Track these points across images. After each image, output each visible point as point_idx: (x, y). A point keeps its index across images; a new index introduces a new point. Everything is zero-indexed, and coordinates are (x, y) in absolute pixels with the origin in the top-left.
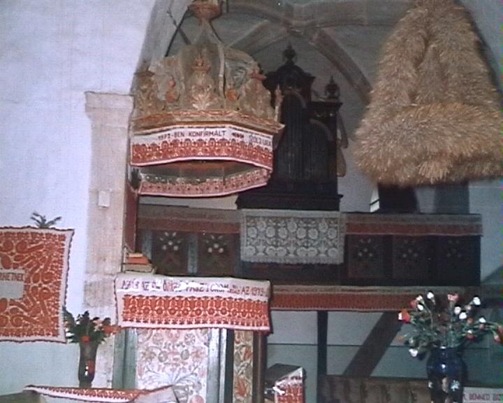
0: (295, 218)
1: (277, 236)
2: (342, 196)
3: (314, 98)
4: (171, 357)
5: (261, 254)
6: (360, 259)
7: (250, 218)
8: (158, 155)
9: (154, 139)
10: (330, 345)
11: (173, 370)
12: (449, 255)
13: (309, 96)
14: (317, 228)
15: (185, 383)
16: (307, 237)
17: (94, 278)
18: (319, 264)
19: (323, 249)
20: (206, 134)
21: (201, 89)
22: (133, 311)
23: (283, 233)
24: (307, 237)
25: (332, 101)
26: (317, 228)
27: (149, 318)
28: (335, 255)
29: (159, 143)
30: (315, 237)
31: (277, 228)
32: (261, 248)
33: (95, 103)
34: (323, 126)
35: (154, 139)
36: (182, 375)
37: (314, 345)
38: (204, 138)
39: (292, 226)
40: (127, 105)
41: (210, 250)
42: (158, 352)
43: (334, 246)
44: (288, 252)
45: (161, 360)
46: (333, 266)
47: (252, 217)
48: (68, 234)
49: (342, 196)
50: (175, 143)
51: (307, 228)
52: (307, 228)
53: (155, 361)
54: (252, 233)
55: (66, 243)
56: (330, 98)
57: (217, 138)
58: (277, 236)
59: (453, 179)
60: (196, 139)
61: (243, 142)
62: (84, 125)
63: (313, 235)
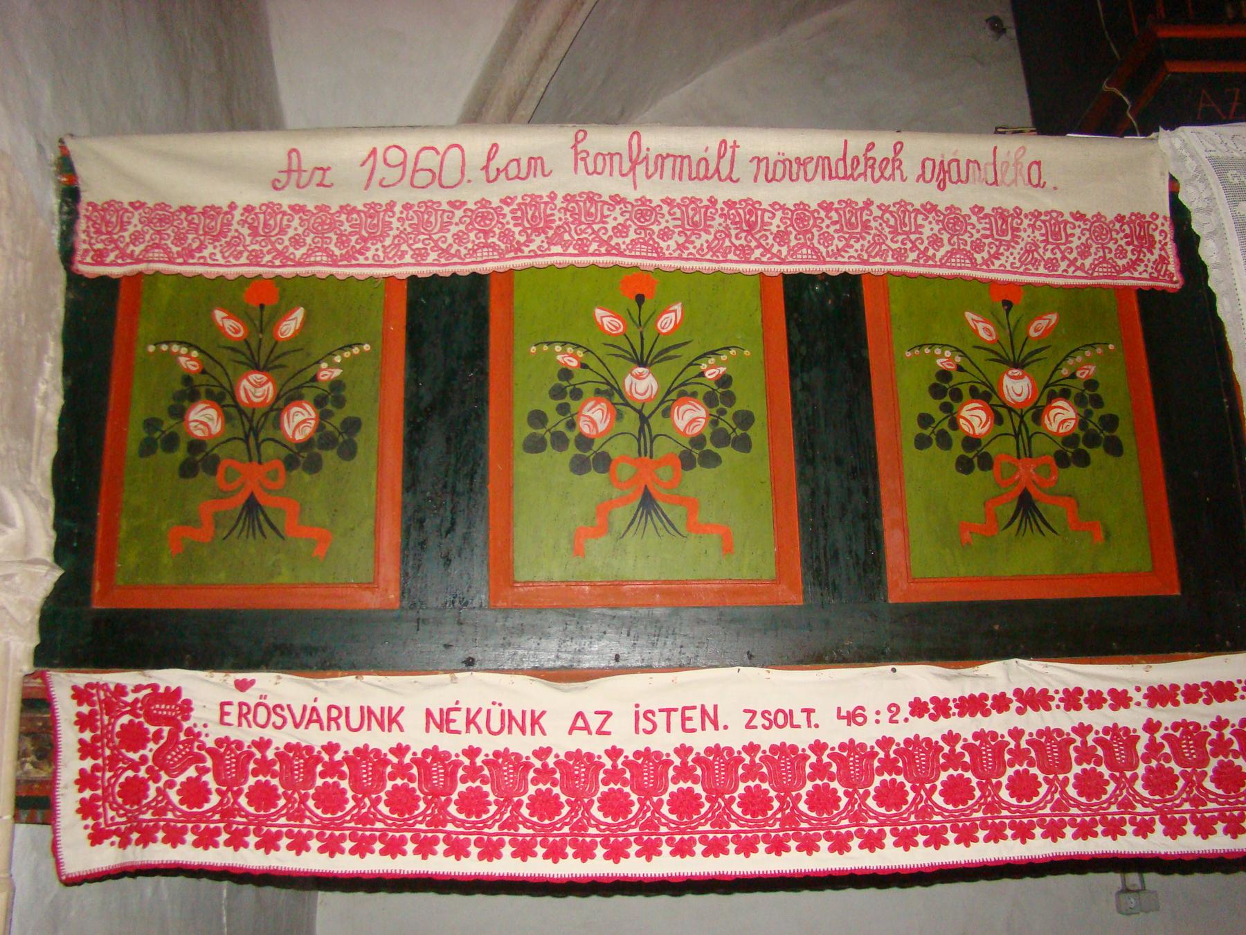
12: (204, 419)
41: (204, 419)
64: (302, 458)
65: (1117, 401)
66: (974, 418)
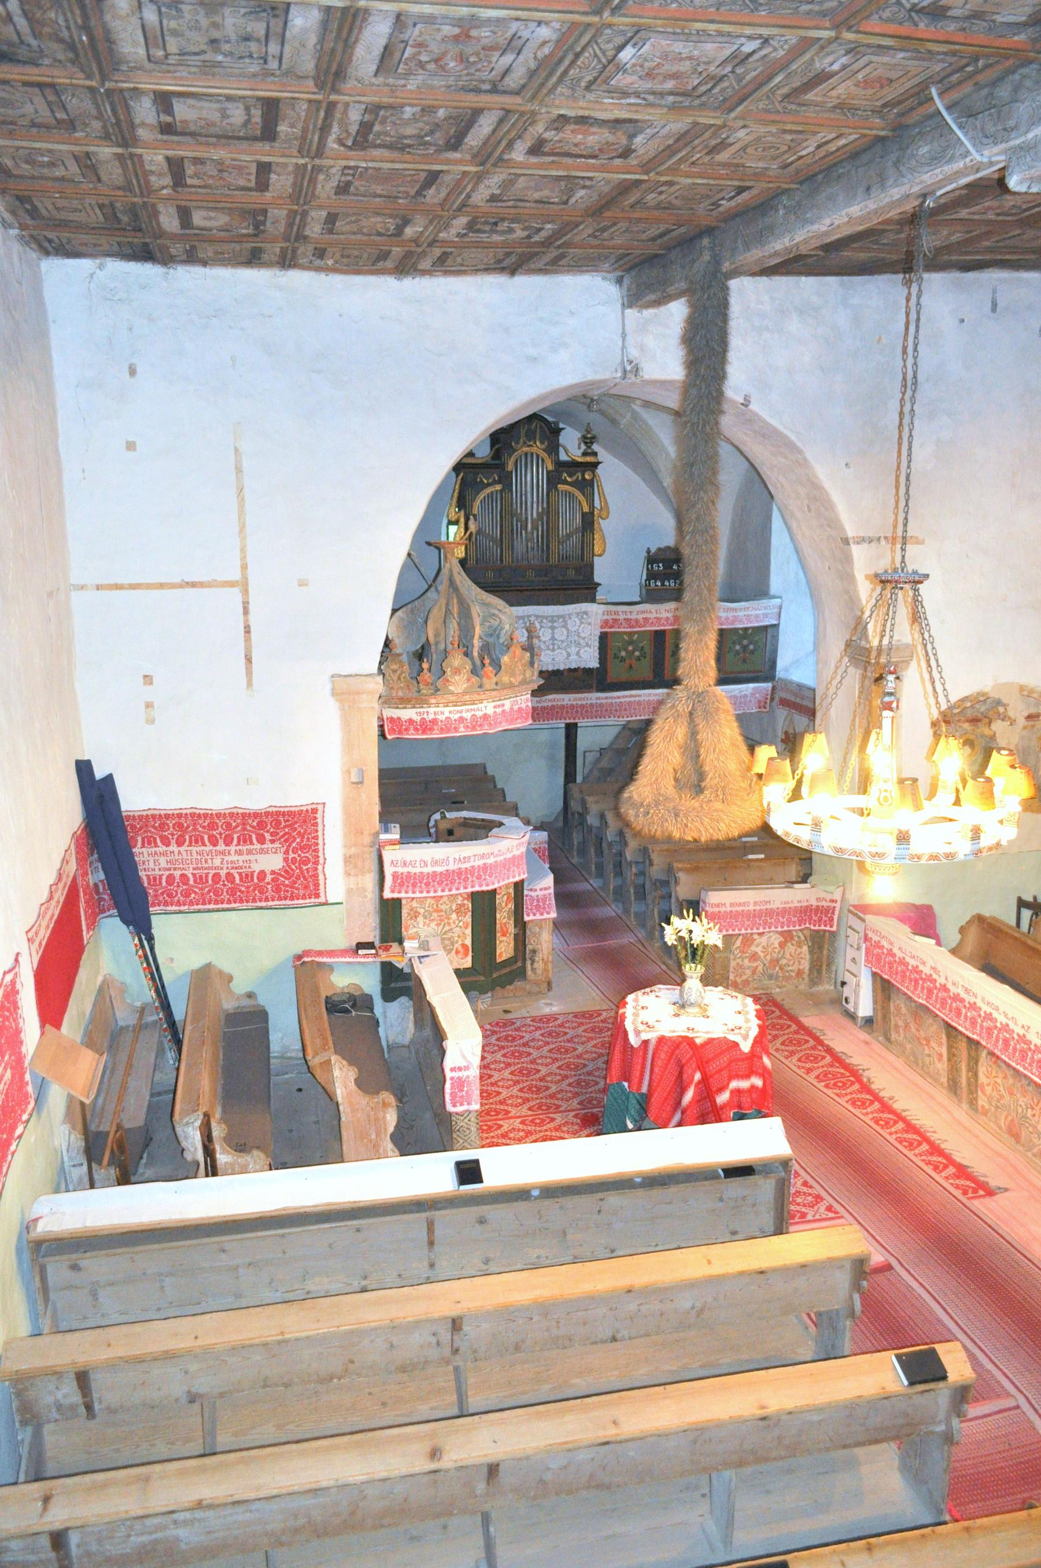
3: (563, 457)
4: (435, 915)
6: (623, 660)
8: (416, 729)
9: (407, 714)
11: (438, 925)
13: (557, 454)
14: (565, 626)
15: (450, 935)
16: (553, 638)
17: (353, 850)
18: (570, 670)
19: (573, 650)
20: (468, 711)
21: (457, 671)
22: (401, 885)
24: (553, 638)
25: (589, 459)
26: (565, 626)
27: (417, 890)
28: (590, 658)
29: (417, 718)
30: (563, 638)
33: (344, 689)
34: (577, 493)
35: (407, 714)
36: (447, 928)
38: (464, 715)
40: (377, 685)
42: (422, 911)
43: (587, 645)
44: (569, 655)
45: (425, 917)
46: (588, 671)
48: (320, 807)
50: (434, 721)
51: (553, 628)
52: (553, 628)
53: (420, 919)
55: (319, 815)
56: (585, 454)
57: (479, 714)
60: (457, 716)
61: (504, 711)
62: (331, 712)
63: (561, 634)
64: (638, 659)
65: (647, 650)
66: (623, 654)
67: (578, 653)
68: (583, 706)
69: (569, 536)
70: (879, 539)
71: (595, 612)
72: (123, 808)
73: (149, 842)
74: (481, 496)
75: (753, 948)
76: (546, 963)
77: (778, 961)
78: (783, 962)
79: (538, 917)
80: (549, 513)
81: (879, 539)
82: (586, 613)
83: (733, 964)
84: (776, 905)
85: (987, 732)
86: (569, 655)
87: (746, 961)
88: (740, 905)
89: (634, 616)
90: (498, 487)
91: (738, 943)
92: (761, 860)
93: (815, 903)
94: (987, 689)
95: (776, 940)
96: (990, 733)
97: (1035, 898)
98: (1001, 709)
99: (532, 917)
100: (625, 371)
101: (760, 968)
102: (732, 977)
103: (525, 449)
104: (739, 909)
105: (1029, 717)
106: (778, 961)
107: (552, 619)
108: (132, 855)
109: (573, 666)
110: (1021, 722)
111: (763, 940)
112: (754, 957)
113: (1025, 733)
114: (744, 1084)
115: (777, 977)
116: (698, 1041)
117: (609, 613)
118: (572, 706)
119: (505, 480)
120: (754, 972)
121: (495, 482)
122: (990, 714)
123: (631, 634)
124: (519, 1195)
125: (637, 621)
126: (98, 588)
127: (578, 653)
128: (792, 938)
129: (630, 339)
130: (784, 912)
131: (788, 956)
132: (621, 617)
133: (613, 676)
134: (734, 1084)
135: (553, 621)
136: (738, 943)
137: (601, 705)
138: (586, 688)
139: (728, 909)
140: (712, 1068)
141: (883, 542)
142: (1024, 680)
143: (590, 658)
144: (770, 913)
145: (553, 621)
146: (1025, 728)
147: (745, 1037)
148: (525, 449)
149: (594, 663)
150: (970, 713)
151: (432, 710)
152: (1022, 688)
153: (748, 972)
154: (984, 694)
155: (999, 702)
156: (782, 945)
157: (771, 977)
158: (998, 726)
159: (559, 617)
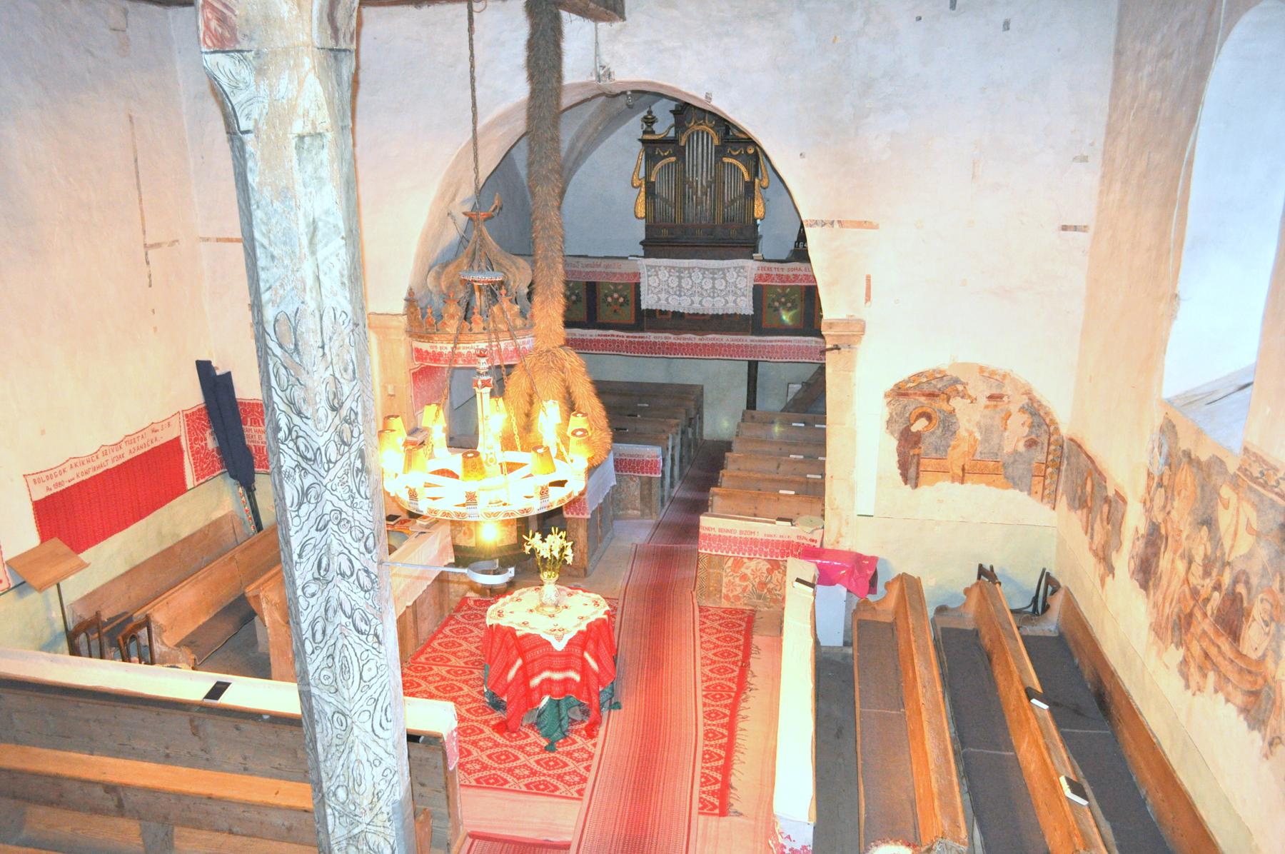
0: (700, 269)
1: (680, 286)
2: (465, 214)
5: (663, 302)
7: (649, 267)
10: (238, 240)
14: (724, 278)
16: (714, 287)
23: (686, 283)
24: (714, 287)
26: (724, 278)
28: (745, 306)
29: (430, 350)
31: (680, 278)
32: (697, 299)
37: (238, 240)
39: (697, 277)
47: (652, 267)
49: (465, 214)
51: (714, 279)
52: (714, 279)
54: (653, 281)
58: (680, 286)
59: (313, 700)
63: (720, 284)
67: (735, 302)
68: (738, 346)
69: (733, 201)
70: (832, 223)
71: (751, 267)
72: (238, 395)
73: (255, 422)
74: (659, 165)
75: (743, 570)
76: (582, 554)
77: (765, 584)
78: (771, 586)
79: (575, 516)
80: (716, 183)
81: (832, 223)
82: (743, 268)
83: (725, 580)
84: (760, 536)
85: (945, 406)
86: (693, 302)
87: (737, 580)
88: (727, 531)
89: (785, 273)
90: (673, 159)
91: (730, 563)
92: (790, 496)
93: (796, 540)
94: (944, 367)
95: (765, 566)
96: (950, 409)
97: (992, 568)
98: (960, 388)
99: (570, 516)
100: (598, 76)
101: (750, 587)
102: (724, 591)
103: (697, 128)
104: (728, 534)
105: (991, 397)
106: (765, 584)
107: (713, 271)
108: (242, 430)
109: (730, 312)
110: (983, 401)
111: (753, 564)
112: (744, 577)
113: (987, 412)
114: (557, 676)
115: (765, 598)
116: (518, 634)
117: (763, 268)
118: (729, 346)
119: (680, 153)
120: (744, 590)
121: (670, 155)
122: (948, 391)
123: (784, 288)
124: (253, 716)
125: (788, 277)
126: (218, 240)
127: (735, 302)
128: (779, 567)
129: (602, 48)
130: (766, 543)
131: (774, 580)
132: (774, 272)
133: (768, 321)
134: (546, 674)
135: (714, 273)
136: (730, 563)
137: (755, 347)
138: (744, 331)
139: (718, 533)
140: (529, 656)
141: (836, 225)
142: (983, 362)
143: (745, 306)
144: (755, 542)
145: (714, 273)
146: (986, 407)
147: (559, 639)
148: (697, 128)
149: (750, 311)
150: (926, 388)
151: (439, 345)
152: (982, 370)
153: (739, 590)
154: (940, 372)
155: (957, 381)
156: (770, 571)
157: (759, 597)
158: (957, 403)
159: (719, 270)
